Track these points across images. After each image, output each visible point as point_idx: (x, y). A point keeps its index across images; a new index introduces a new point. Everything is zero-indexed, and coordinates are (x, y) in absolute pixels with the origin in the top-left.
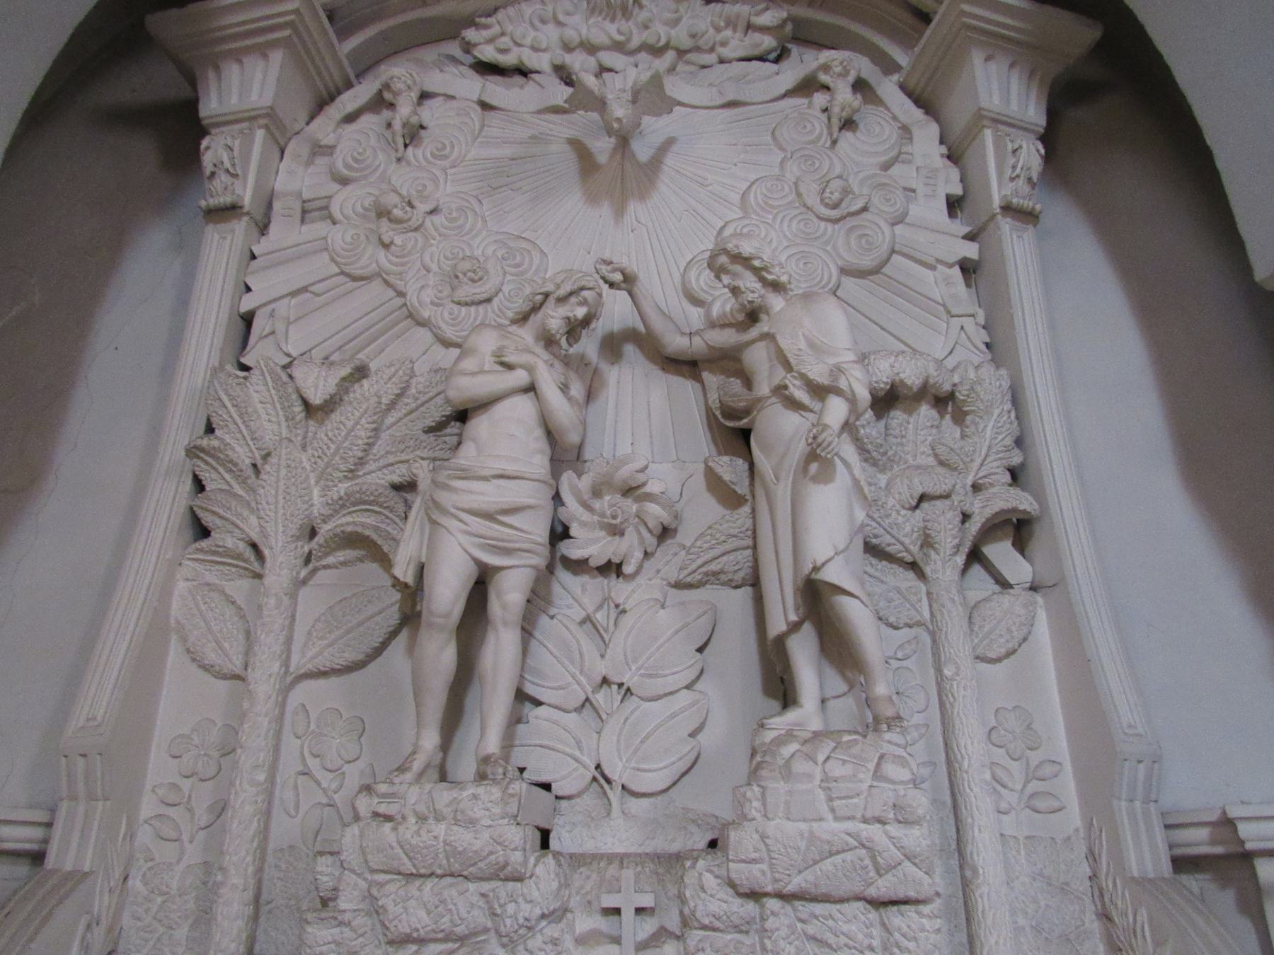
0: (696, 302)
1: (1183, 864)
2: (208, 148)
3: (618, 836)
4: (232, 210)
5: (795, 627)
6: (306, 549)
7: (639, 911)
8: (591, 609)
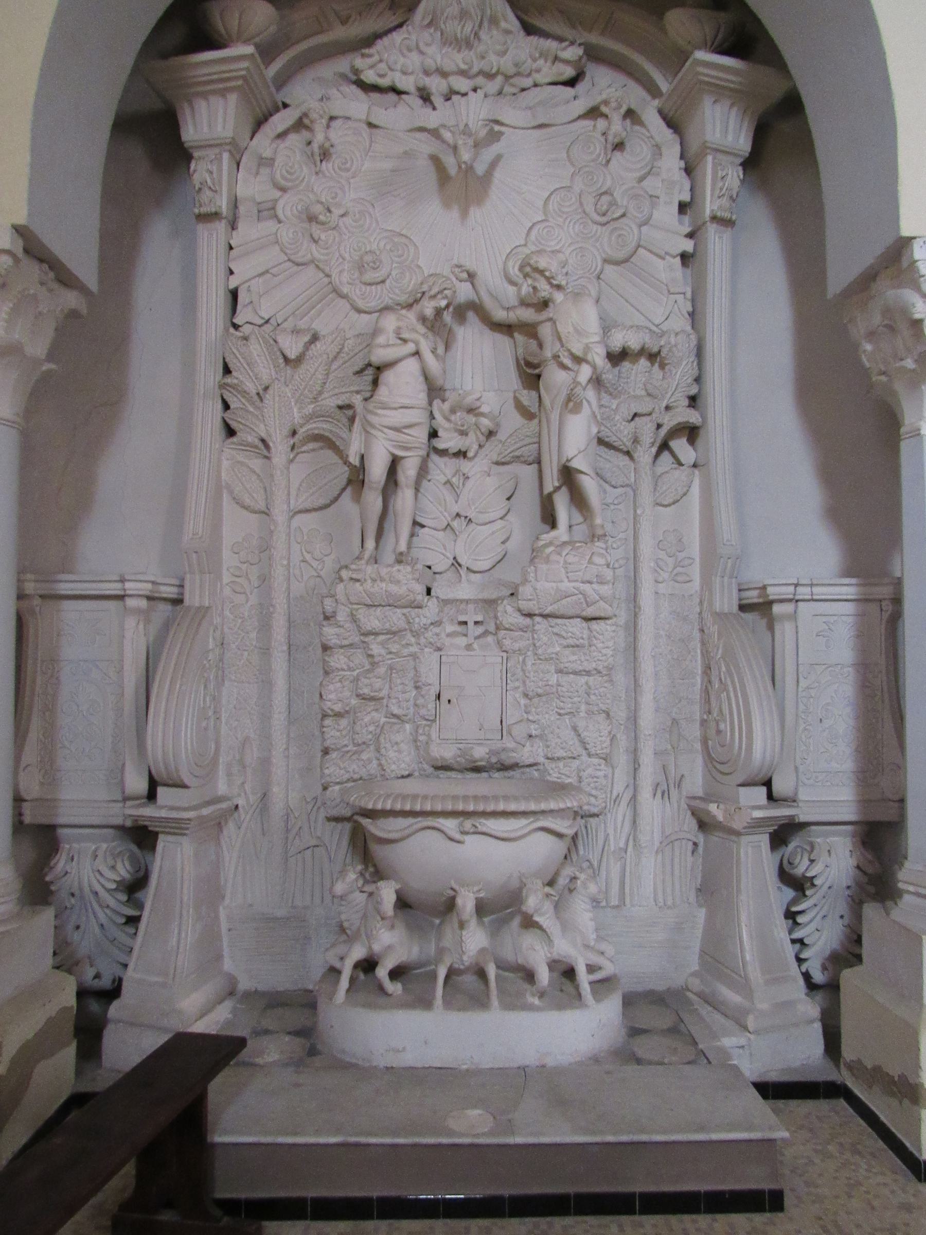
0: (513, 283)
1: (743, 608)
2: (195, 171)
3: (465, 590)
4: (214, 216)
5: (557, 489)
6: (292, 442)
7: (476, 623)
8: (449, 477)
